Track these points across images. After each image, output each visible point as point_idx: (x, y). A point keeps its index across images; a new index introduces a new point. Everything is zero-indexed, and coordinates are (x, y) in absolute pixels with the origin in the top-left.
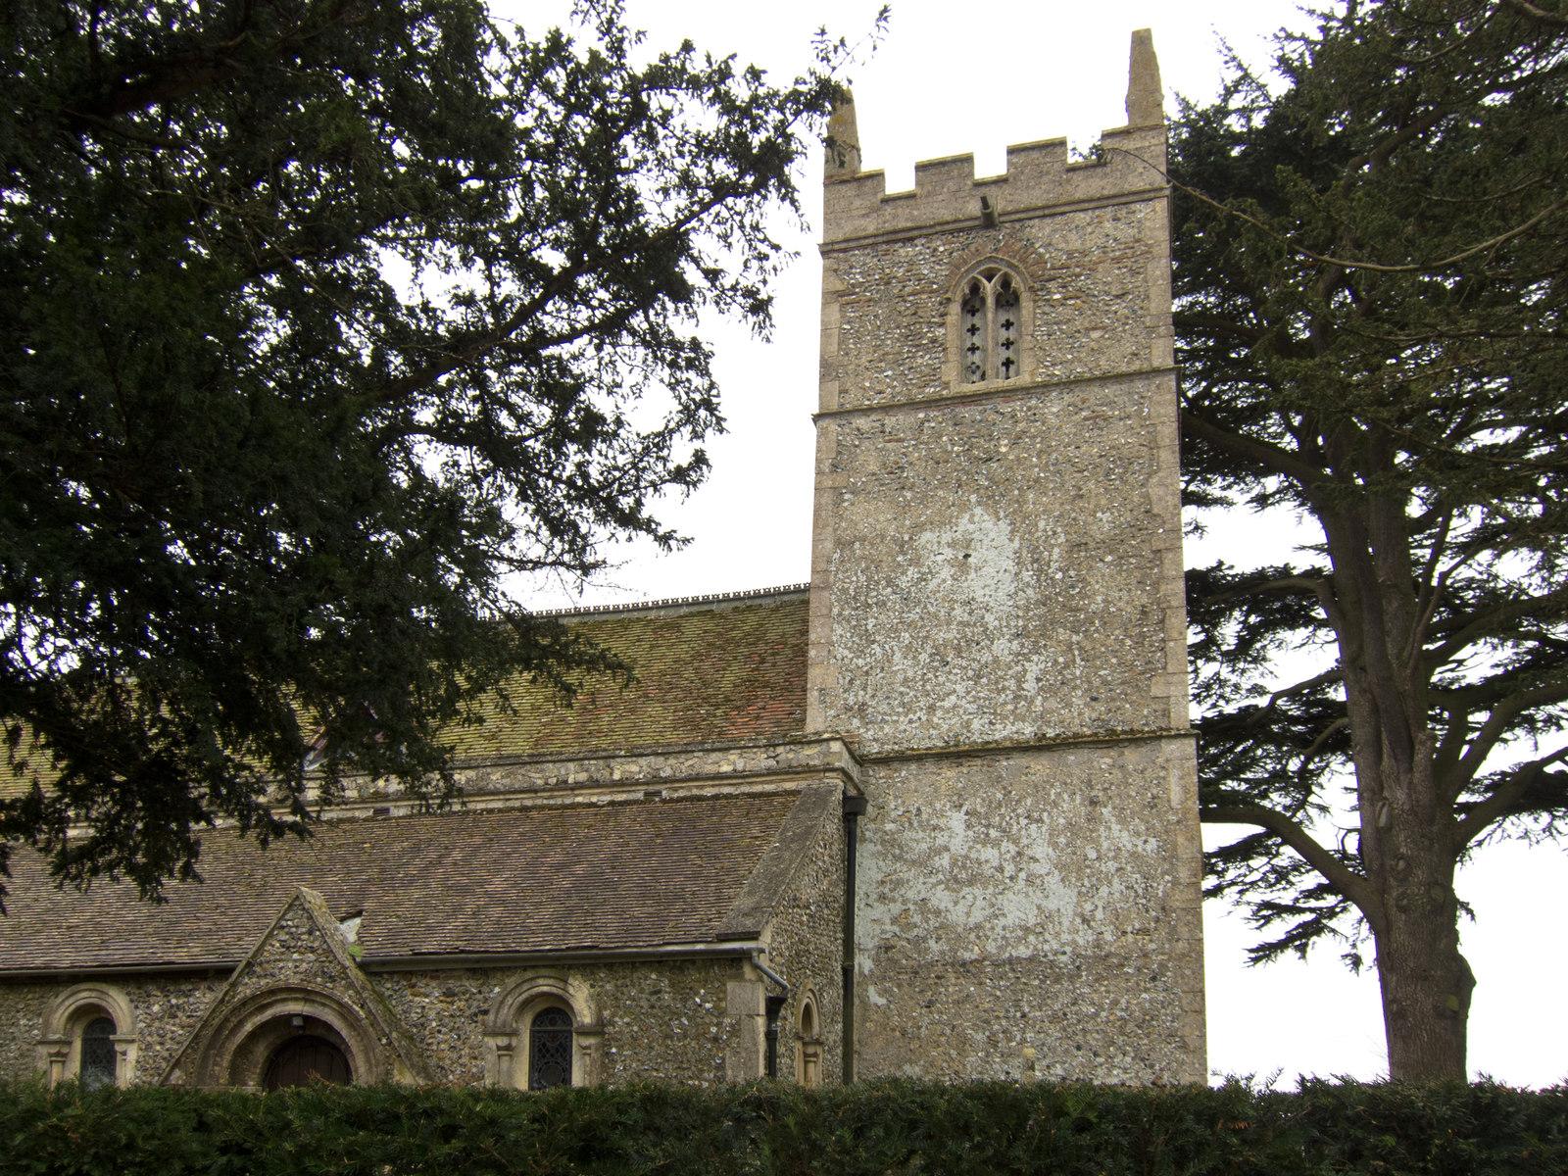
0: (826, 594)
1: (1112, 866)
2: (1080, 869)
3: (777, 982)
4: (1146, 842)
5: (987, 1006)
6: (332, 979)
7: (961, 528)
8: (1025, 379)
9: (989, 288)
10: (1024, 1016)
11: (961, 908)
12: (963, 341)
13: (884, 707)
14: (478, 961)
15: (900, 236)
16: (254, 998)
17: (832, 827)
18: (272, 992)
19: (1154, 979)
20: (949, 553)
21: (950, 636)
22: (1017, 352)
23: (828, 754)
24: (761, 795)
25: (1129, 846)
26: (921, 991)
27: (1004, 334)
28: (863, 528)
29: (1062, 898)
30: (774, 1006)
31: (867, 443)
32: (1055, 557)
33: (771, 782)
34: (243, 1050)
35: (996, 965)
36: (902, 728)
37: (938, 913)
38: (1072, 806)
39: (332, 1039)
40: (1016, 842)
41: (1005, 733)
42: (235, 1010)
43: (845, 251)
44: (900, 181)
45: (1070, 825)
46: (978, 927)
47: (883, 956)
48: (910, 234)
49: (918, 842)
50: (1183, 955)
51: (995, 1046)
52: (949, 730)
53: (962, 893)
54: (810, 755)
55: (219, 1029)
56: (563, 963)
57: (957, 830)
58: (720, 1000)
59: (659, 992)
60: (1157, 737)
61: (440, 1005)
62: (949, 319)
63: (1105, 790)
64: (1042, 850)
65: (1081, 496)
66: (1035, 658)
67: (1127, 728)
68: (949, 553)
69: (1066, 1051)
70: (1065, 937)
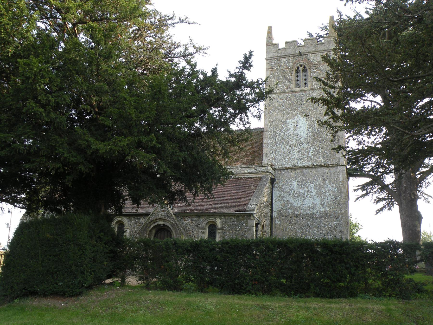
0: (267, 133)
1: (328, 194)
2: (321, 195)
3: (258, 220)
4: (335, 189)
5: (301, 224)
6: (169, 217)
7: (296, 119)
8: (308, 88)
9: (301, 68)
10: (309, 226)
11: (296, 202)
12: (296, 79)
13: (279, 158)
14: (198, 214)
15: (282, 57)
16: (153, 220)
17: (268, 185)
18: (157, 219)
19: (337, 219)
20: (293, 124)
21: (293, 143)
22: (307, 81)
23: (268, 169)
24: (253, 178)
25: (332, 189)
26: (287, 221)
27: (304, 78)
28: (275, 119)
29: (317, 201)
30: (257, 225)
31: (275, 100)
32: (316, 126)
33: (255, 175)
34: (151, 231)
35: (303, 215)
36: (283, 162)
37: (291, 203)
38: (320, 180)
39: (169, 229)
40: (307, 188)
41: (305, 164)
42: (149, 223)
43: (271, 59)
44: (282, 45)
45: (319, 185)
46: (300, 207)
47: (279, 213)
48: (284, 57)
49: (287, 188)
50: (343, 214)
51: (303, 233)
52: (293, 163)
53: (296, 199)
54: (264, 169)
55: (146, 227)
56: (215, 215)
57: (295, 185)
58: (246, 223)
59: (234, 221)
60: (337, 165)
61: (190, 223)
62: (293, 74)
63: (326, 177)
64: (313, 190)
65: (321, 113)
66: (312, 148)
67: (331, 164)
68: (293, 124)
69: (318, 234)
70: (318, 209)
